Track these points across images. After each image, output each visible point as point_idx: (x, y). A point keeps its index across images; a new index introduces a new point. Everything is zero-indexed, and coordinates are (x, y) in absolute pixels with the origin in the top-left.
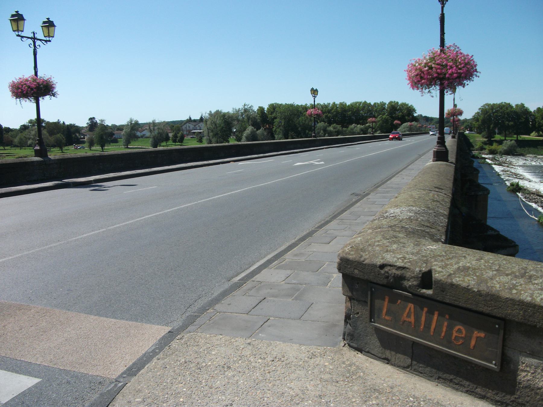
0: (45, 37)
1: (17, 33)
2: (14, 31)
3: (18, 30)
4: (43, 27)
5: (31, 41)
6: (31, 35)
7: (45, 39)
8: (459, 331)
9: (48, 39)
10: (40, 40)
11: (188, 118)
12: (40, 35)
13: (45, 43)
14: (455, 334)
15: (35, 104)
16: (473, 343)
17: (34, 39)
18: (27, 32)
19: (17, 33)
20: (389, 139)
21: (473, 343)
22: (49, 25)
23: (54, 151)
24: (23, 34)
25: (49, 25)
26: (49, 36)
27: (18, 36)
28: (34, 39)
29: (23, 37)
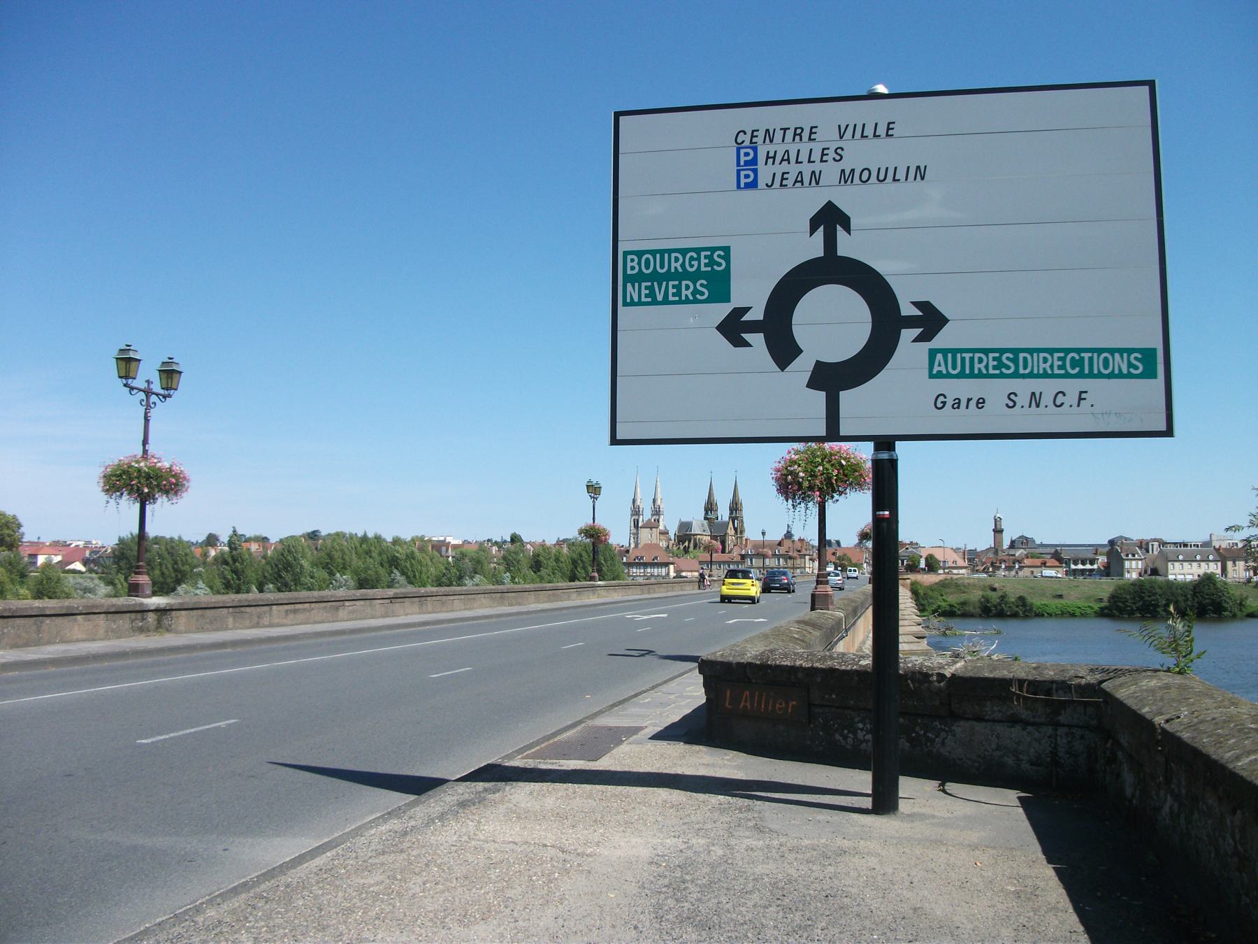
0: (162, 388)
1: (125, 382)
2: (120, 377)
3: (127, 377)
4: (120, 362)
5: (142, 395)
6: (143, 385)
7: (162, 392)
8: (781, 704)
9: (166, 393)
10: (157, 395)
11: (1207, 538)
12: (156, 387)
13: (163, 400)
14: (777, 705)
15: (906, 532)
16: (790, 710)
17: (148, 393)
18: (139, 382)
19: (124, 381)
20: (731, 522)
21: (790, 710)
22: (170, 375)
23: (301, 859)
24: (134, 383)
25: (170, 375)
26: (167, 389)
27: (125, 385)
28: (148, 393)
29: (132, 388)
